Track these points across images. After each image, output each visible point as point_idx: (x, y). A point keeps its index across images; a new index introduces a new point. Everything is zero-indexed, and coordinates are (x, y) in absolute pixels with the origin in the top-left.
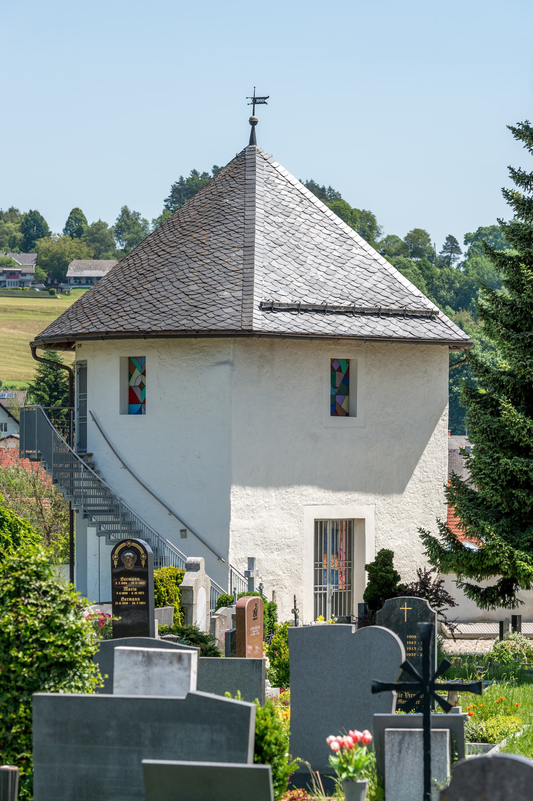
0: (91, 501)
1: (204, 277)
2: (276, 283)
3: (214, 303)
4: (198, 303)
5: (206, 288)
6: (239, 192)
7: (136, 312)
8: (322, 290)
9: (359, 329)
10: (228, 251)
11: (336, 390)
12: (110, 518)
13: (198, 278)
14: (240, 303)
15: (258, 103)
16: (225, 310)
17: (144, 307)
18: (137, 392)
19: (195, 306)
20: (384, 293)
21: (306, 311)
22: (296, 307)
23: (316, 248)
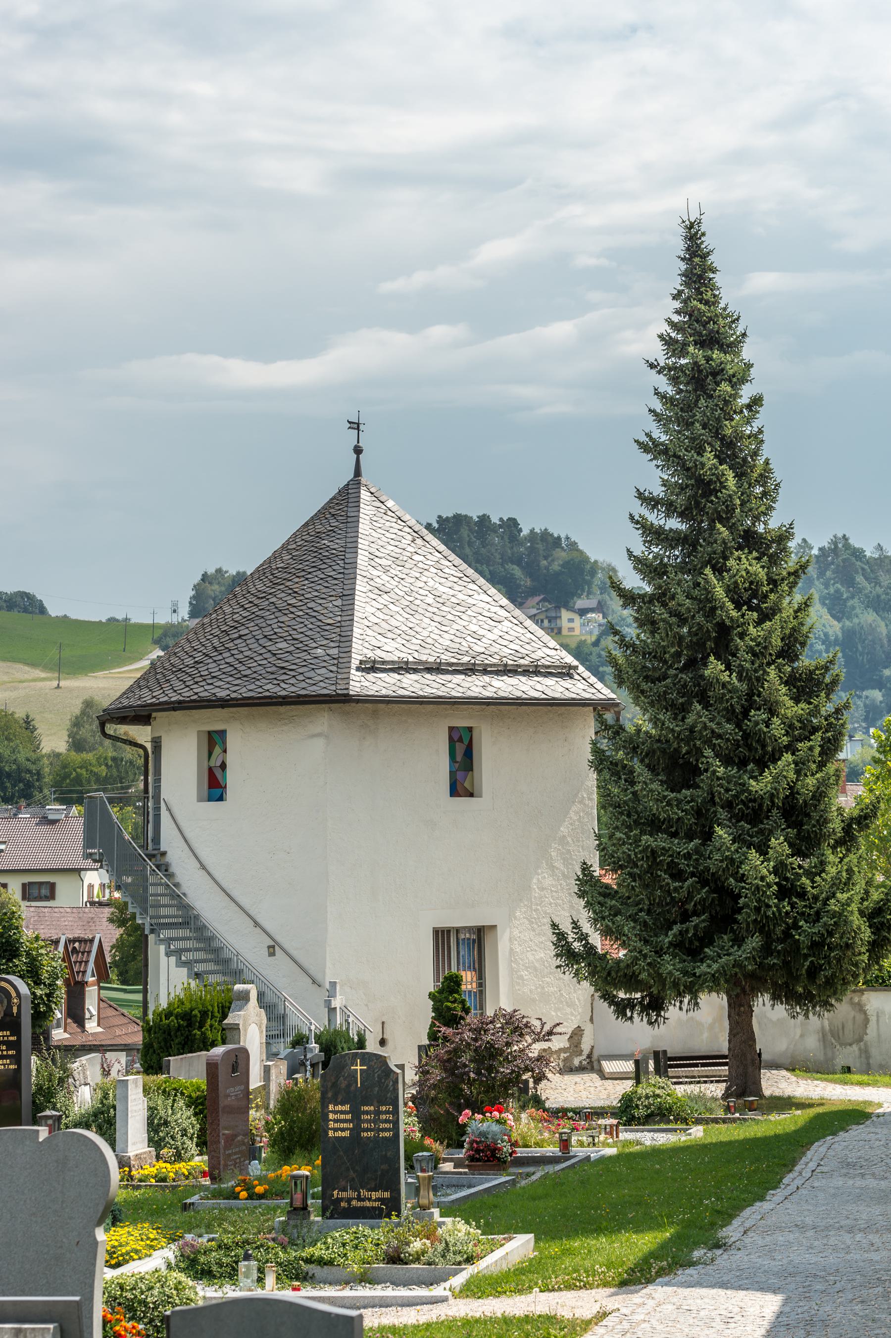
0: (163, 911)
1: (295, 632)
3: (304, 663)
4: (287, 664)
5: (297, 646)
6: (340, 532)
7: (214, 677)
8: (436, 645)
9: (481, 690)
10: (324, 601)
11: (457, 765)
12: (181, 933)
13: (287, 634)
14: (336, 662)
16: (318, 671)
17: (224, 670)
18: (218, 773)
19: (283, 668)
20: (512, 646)
21: (416, 671)
22: (470, 667)
23: (430, 595)
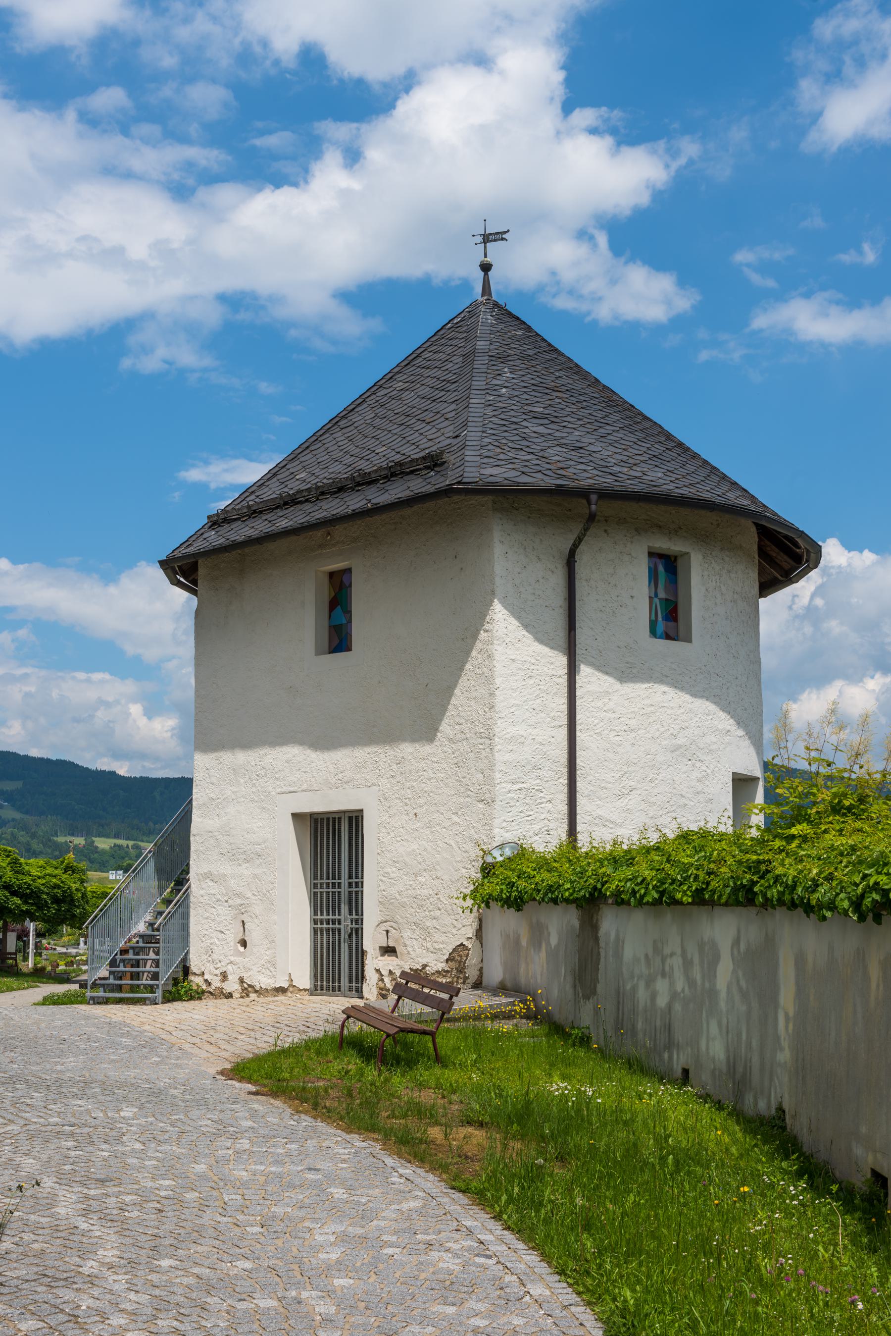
15: (491, 241)
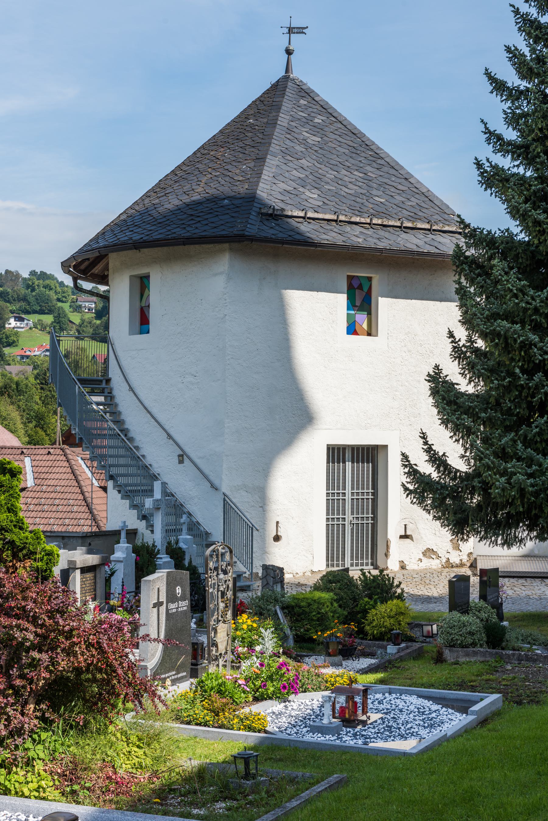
2: (286, 194)
15: (294, 33)
19: (192, 215)
